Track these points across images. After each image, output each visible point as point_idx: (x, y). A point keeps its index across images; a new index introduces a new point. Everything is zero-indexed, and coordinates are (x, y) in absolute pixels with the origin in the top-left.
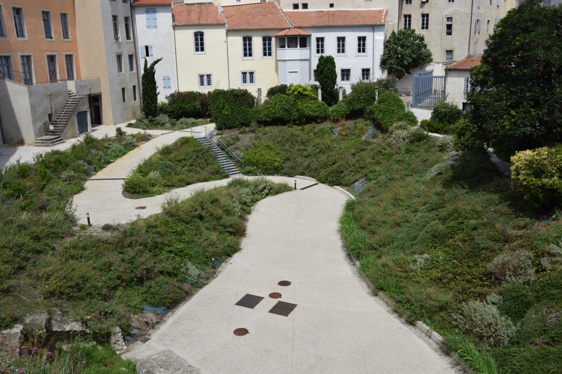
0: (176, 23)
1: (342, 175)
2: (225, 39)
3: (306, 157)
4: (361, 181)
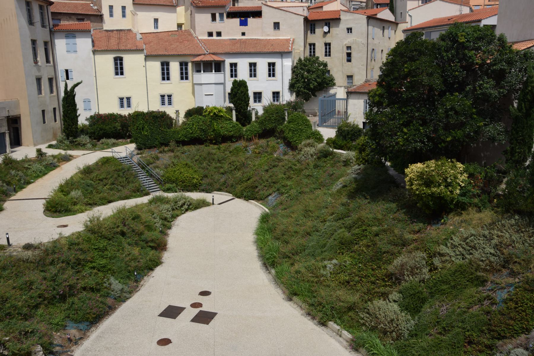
0: (96, 48)
1: (257, 190)
2: (144, 64)
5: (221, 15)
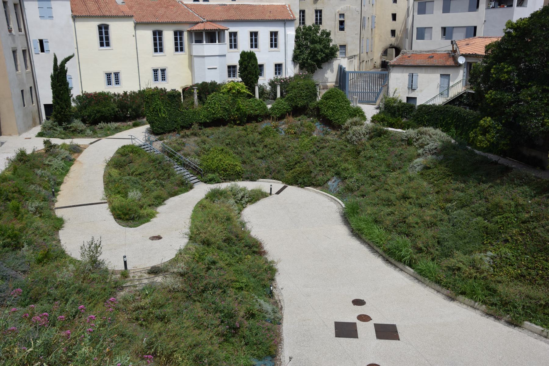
0: (75, 14)
1: (313, 175)
2: (134, 33)
4: (333, 180)
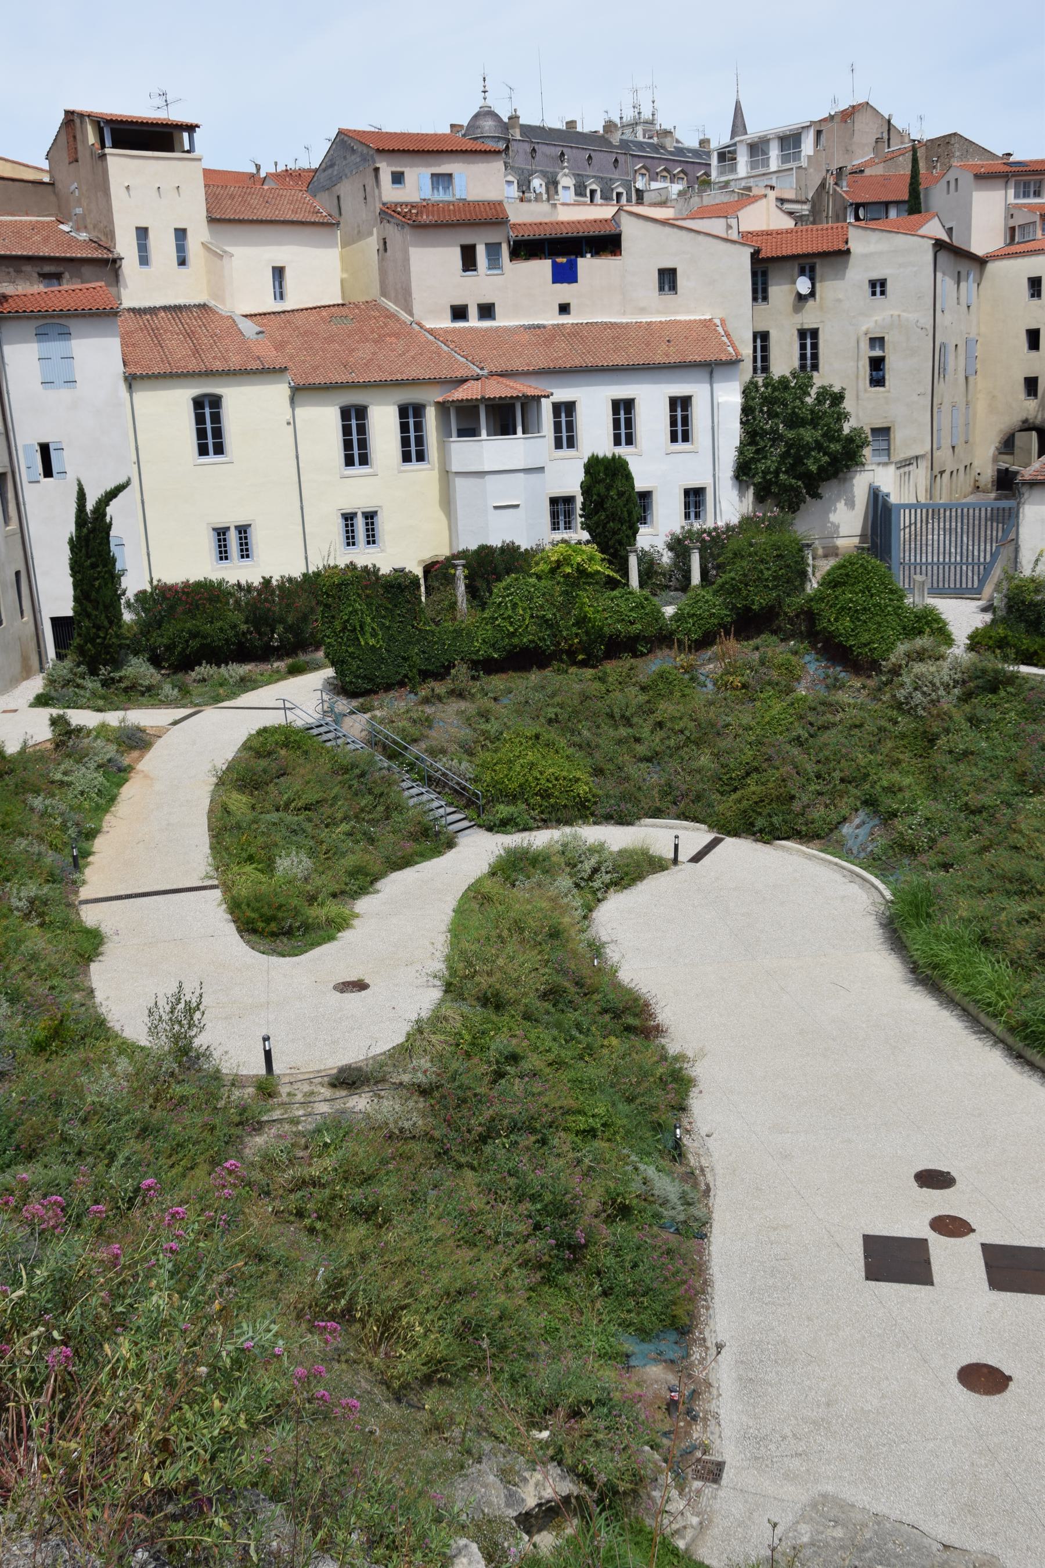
0: (133, 370)
1: (796, 806)
2: (289, 416)
3: (649, 760)
5: (493, 250)
